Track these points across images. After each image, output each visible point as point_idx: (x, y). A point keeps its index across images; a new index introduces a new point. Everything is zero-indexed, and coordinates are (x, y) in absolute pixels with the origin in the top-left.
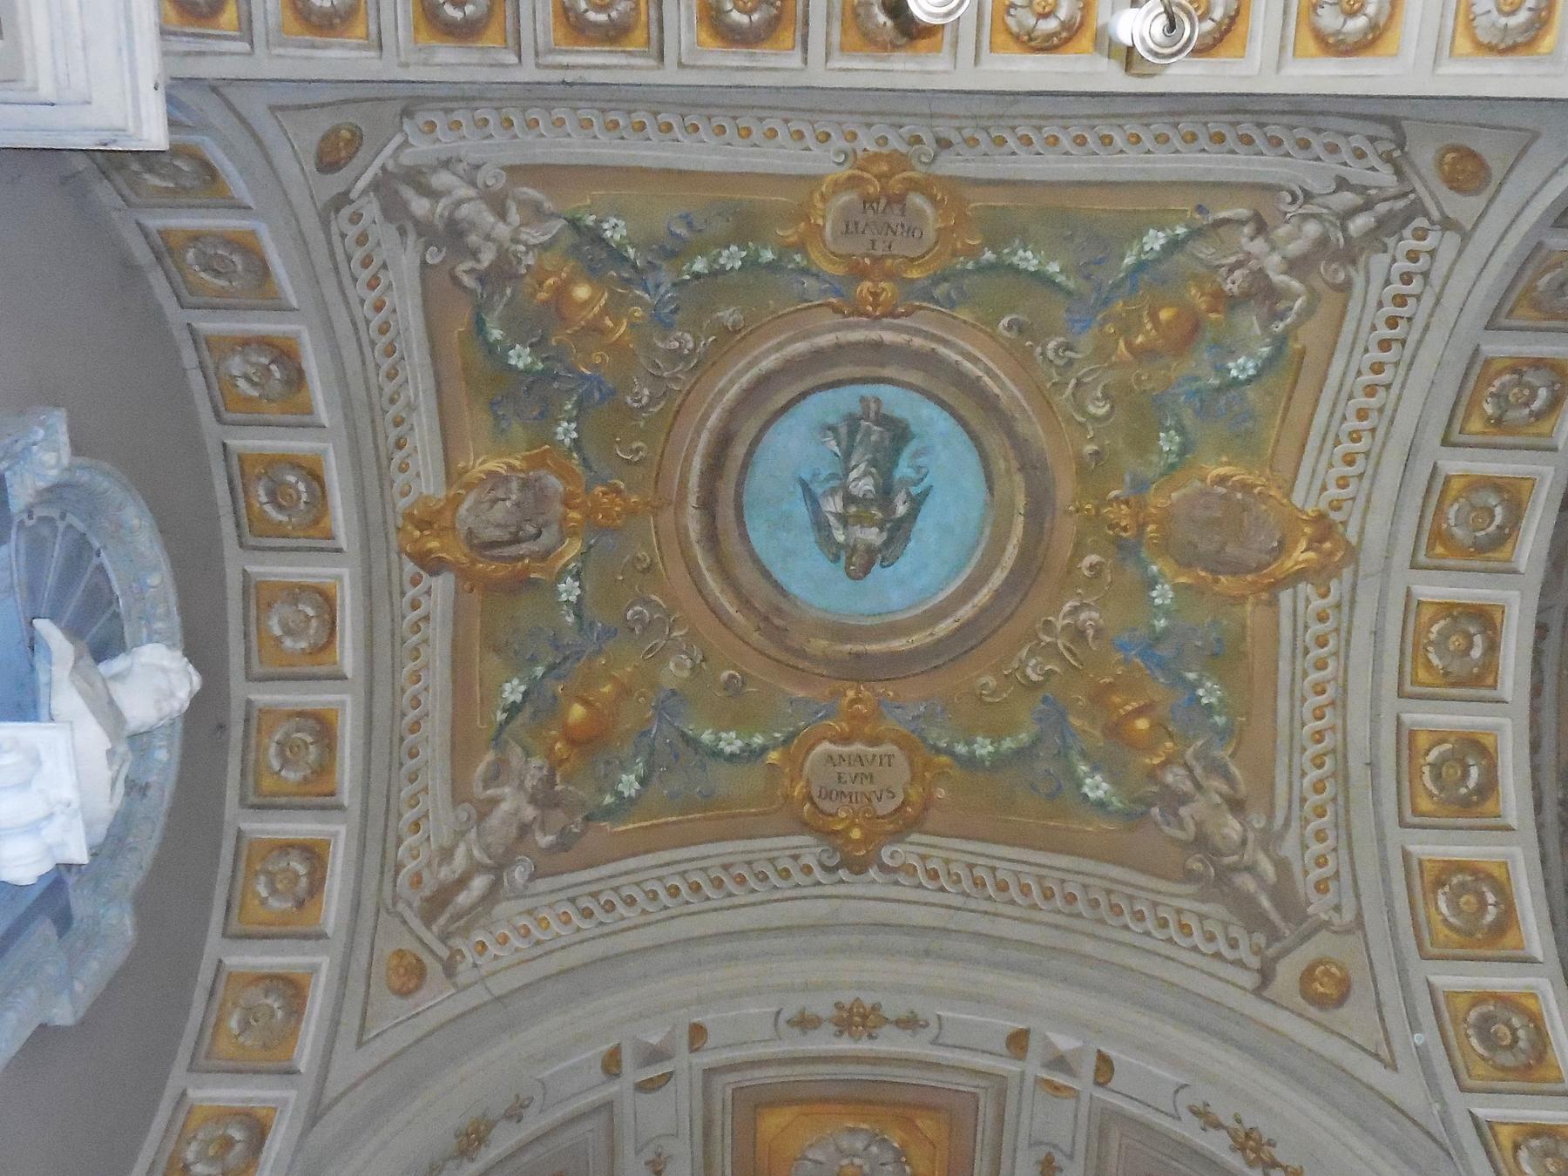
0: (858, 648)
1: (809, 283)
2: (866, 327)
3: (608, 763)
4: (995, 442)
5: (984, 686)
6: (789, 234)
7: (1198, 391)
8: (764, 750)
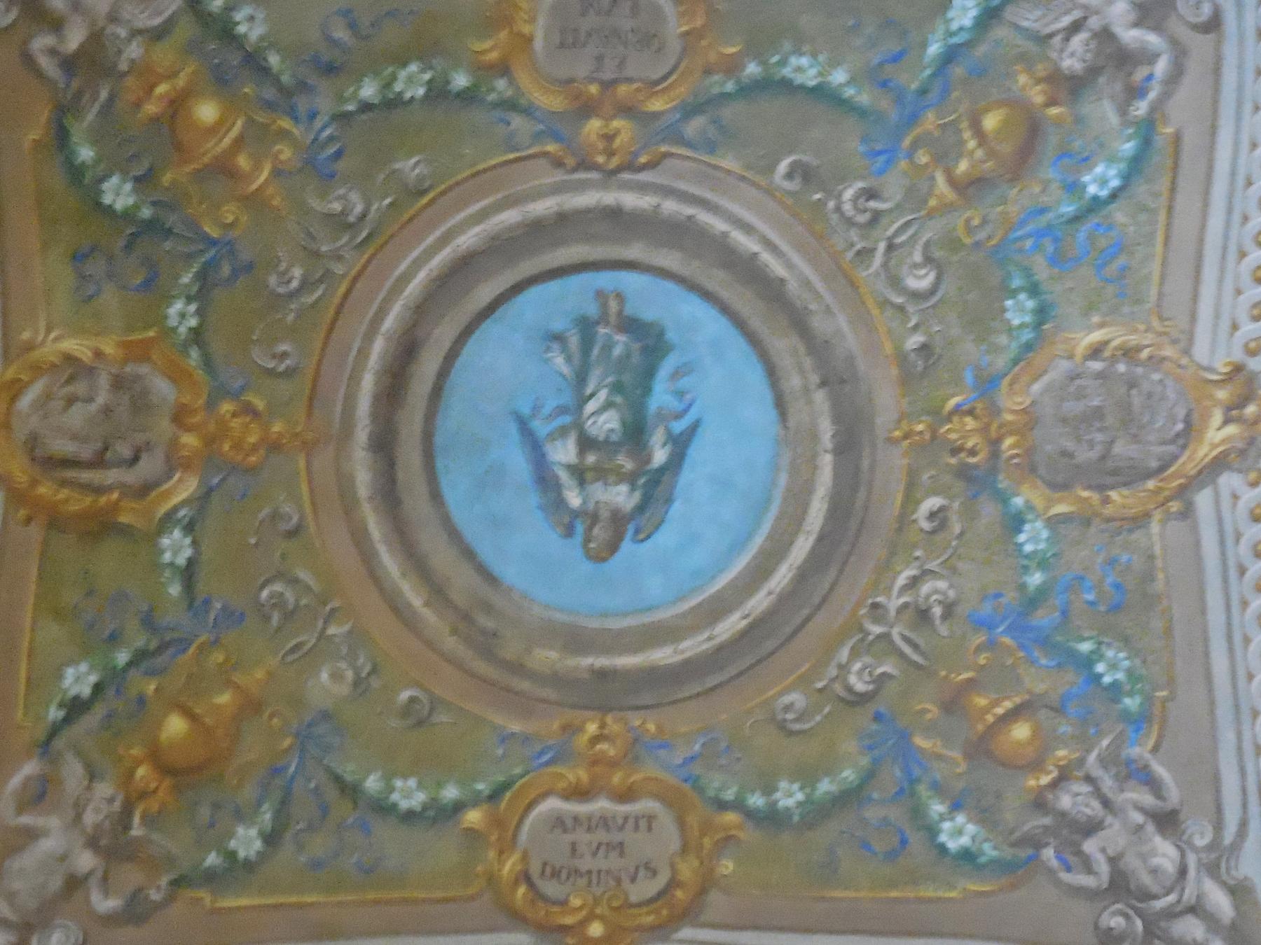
0: (602, 662)
1: (517, 121)
2: (604, 186)
3: (216, 806)
4: (783, 345)
5: (787, 708)
6: (489, 48)
7: (1049, 227)
8: (458, 808)
